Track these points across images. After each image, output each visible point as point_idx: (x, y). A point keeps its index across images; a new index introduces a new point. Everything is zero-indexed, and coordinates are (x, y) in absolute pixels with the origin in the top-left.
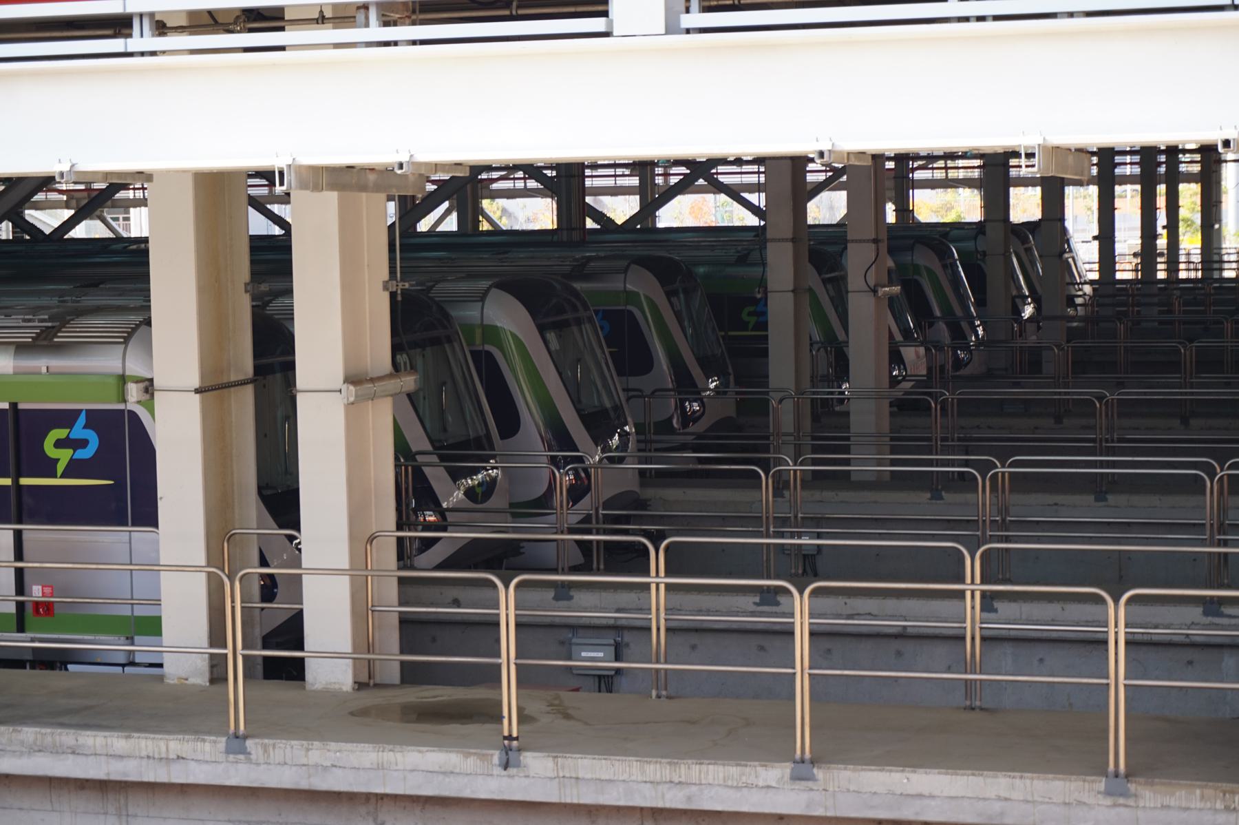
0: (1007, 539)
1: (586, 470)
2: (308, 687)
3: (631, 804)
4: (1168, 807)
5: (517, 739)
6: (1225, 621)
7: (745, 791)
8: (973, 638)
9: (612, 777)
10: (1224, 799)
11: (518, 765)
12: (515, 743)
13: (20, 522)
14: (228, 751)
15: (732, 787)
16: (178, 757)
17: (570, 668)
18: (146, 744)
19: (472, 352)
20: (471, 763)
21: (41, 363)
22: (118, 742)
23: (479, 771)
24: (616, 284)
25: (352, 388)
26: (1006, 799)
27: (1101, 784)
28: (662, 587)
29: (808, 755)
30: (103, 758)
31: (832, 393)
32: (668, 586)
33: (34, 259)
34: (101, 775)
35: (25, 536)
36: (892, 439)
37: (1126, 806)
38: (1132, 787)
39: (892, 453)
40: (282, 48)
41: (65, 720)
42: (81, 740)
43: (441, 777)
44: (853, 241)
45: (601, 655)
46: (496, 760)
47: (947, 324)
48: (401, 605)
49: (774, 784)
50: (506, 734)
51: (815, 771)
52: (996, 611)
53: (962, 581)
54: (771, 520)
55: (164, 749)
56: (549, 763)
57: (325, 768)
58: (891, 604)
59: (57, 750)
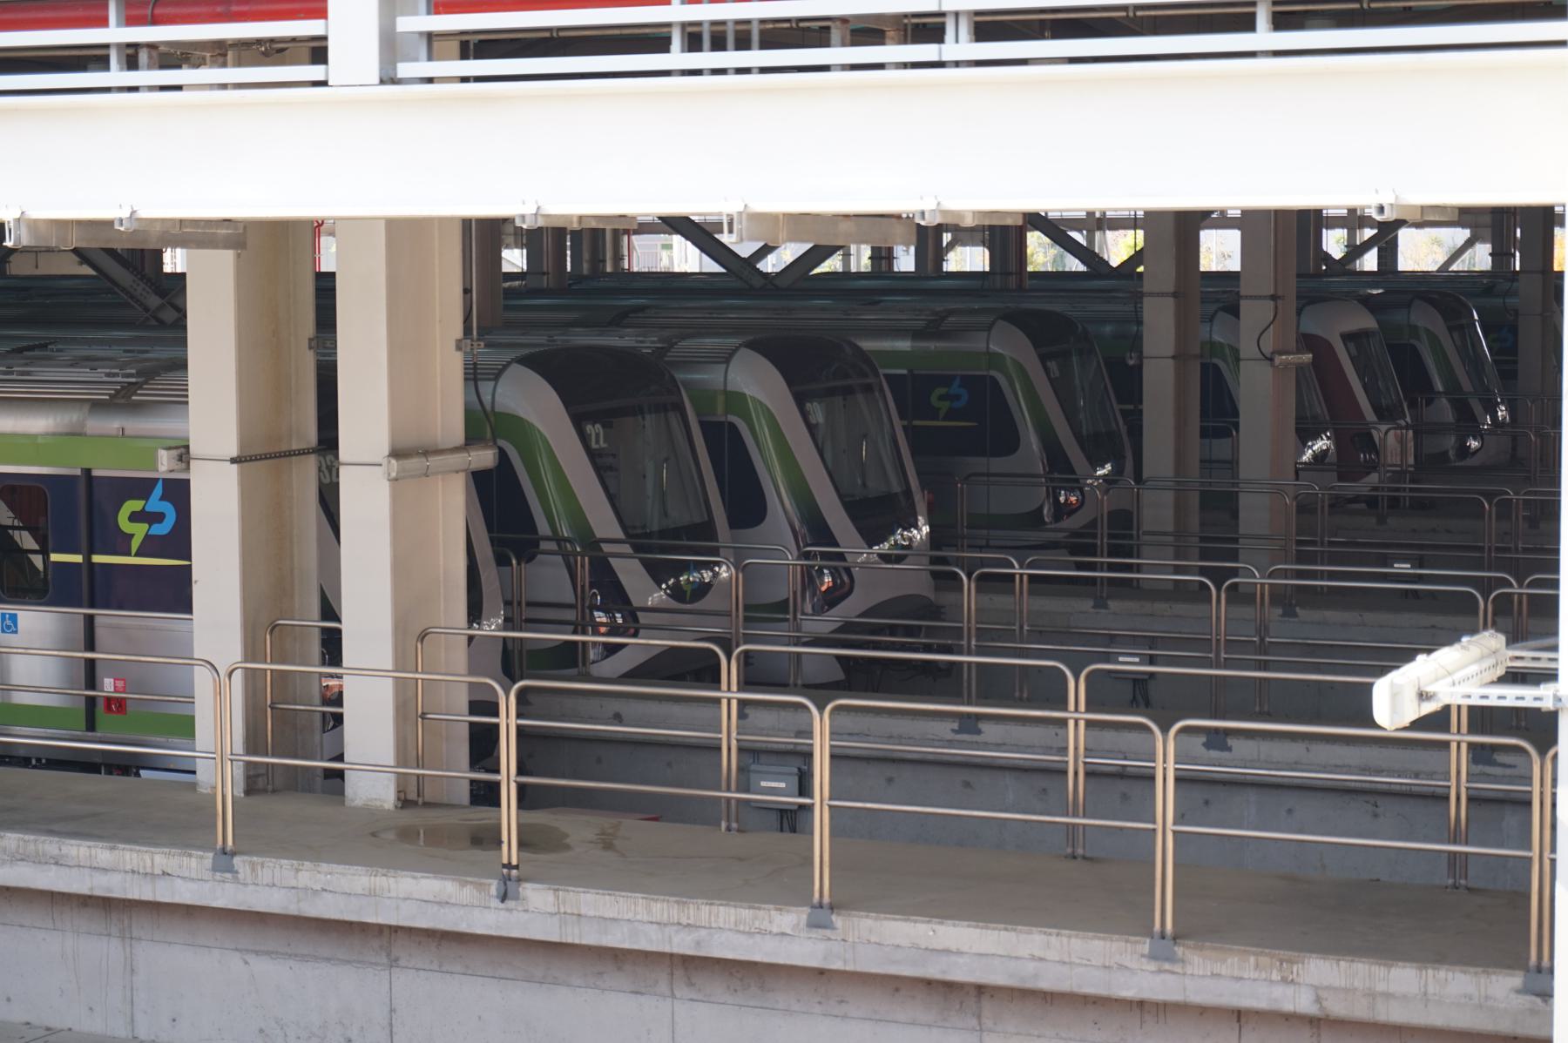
0: (1264, 666)
1: (848, 570)
2: (347, 803)
3: (635, 947)
4: (1219, 975)
5: (517, 867)
6: (1498, 771)
7: (758, 937)
8: (1076, 773)
9: (615, 915)
10: (1281, 970)
11: (517, 898)
12: (514, 872)
13: (92, 606)
14: (215, 869)
15: (744, 933)
16: (164, 873)
17: (748, 801)
18: (131, 856)
19: (702, 424)
20: (467, 894)
21: (112, 424)
22: (102, 854)
23: (476, 902)
24: (977, 343)
25: (394, 461)
26: (1041, 959)
27: (1145, 946)
28: (1082, 724)
29: (826, 899)
30: (87, 871)
31: (1411, 490)
32: (1089, 723)
33: (96, 303)
34: (85, 891)
35: (98, 621)
36: (1203, 539)
37: (1173, 973)
38: (1179, 951)
39: (1201, 559)
40: (179, 88)
41: (56, 827)
42: (65, 850)
43: (436, 908)
44: (1246, 297)
45: (783, 785)
46: (493, 890)
47: (1449, 400)
48: (471, 713)
49: (789, 931)
50: (505, 861)
51: (834, 918)
52: (1229, 749)
53: (1065, 709)
54: (973, 632)
55: (149, 863)
56: (550, 896)
57: (315, 892)
58: (1323, 752)
59: (39, 860)
